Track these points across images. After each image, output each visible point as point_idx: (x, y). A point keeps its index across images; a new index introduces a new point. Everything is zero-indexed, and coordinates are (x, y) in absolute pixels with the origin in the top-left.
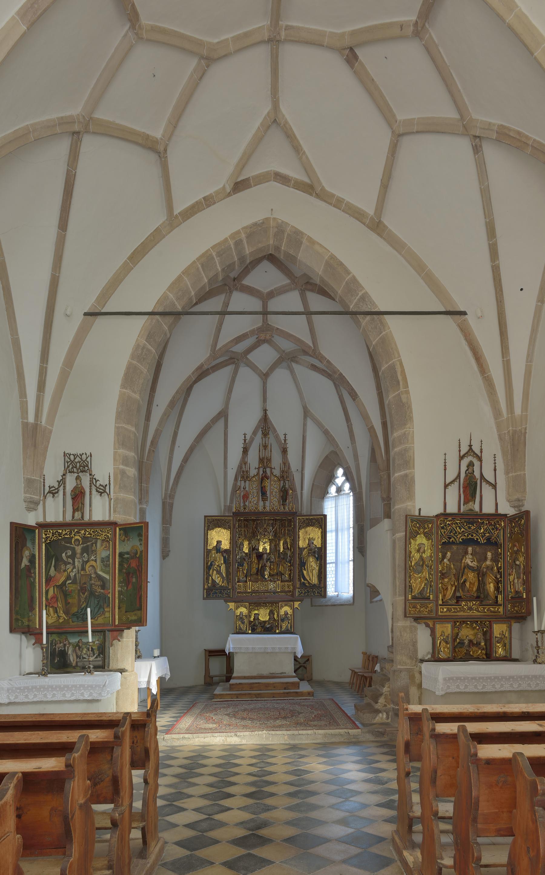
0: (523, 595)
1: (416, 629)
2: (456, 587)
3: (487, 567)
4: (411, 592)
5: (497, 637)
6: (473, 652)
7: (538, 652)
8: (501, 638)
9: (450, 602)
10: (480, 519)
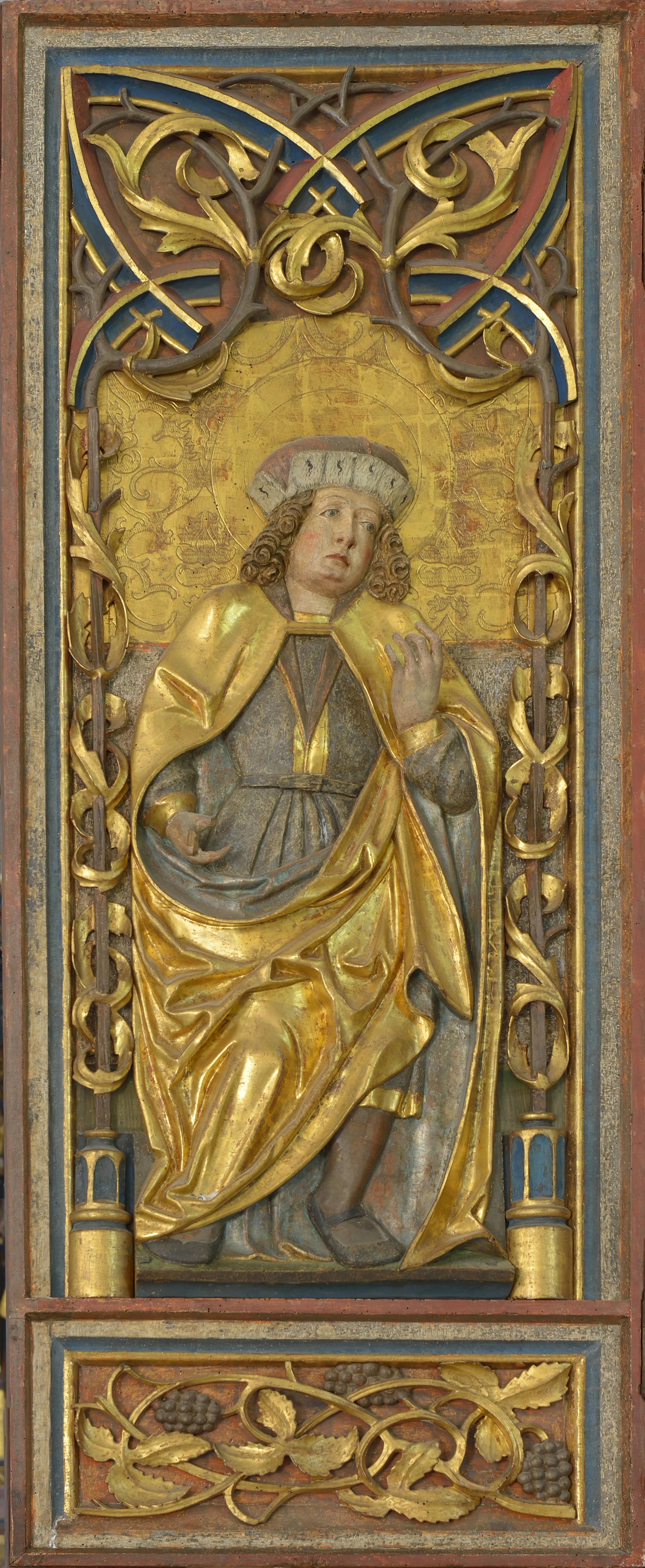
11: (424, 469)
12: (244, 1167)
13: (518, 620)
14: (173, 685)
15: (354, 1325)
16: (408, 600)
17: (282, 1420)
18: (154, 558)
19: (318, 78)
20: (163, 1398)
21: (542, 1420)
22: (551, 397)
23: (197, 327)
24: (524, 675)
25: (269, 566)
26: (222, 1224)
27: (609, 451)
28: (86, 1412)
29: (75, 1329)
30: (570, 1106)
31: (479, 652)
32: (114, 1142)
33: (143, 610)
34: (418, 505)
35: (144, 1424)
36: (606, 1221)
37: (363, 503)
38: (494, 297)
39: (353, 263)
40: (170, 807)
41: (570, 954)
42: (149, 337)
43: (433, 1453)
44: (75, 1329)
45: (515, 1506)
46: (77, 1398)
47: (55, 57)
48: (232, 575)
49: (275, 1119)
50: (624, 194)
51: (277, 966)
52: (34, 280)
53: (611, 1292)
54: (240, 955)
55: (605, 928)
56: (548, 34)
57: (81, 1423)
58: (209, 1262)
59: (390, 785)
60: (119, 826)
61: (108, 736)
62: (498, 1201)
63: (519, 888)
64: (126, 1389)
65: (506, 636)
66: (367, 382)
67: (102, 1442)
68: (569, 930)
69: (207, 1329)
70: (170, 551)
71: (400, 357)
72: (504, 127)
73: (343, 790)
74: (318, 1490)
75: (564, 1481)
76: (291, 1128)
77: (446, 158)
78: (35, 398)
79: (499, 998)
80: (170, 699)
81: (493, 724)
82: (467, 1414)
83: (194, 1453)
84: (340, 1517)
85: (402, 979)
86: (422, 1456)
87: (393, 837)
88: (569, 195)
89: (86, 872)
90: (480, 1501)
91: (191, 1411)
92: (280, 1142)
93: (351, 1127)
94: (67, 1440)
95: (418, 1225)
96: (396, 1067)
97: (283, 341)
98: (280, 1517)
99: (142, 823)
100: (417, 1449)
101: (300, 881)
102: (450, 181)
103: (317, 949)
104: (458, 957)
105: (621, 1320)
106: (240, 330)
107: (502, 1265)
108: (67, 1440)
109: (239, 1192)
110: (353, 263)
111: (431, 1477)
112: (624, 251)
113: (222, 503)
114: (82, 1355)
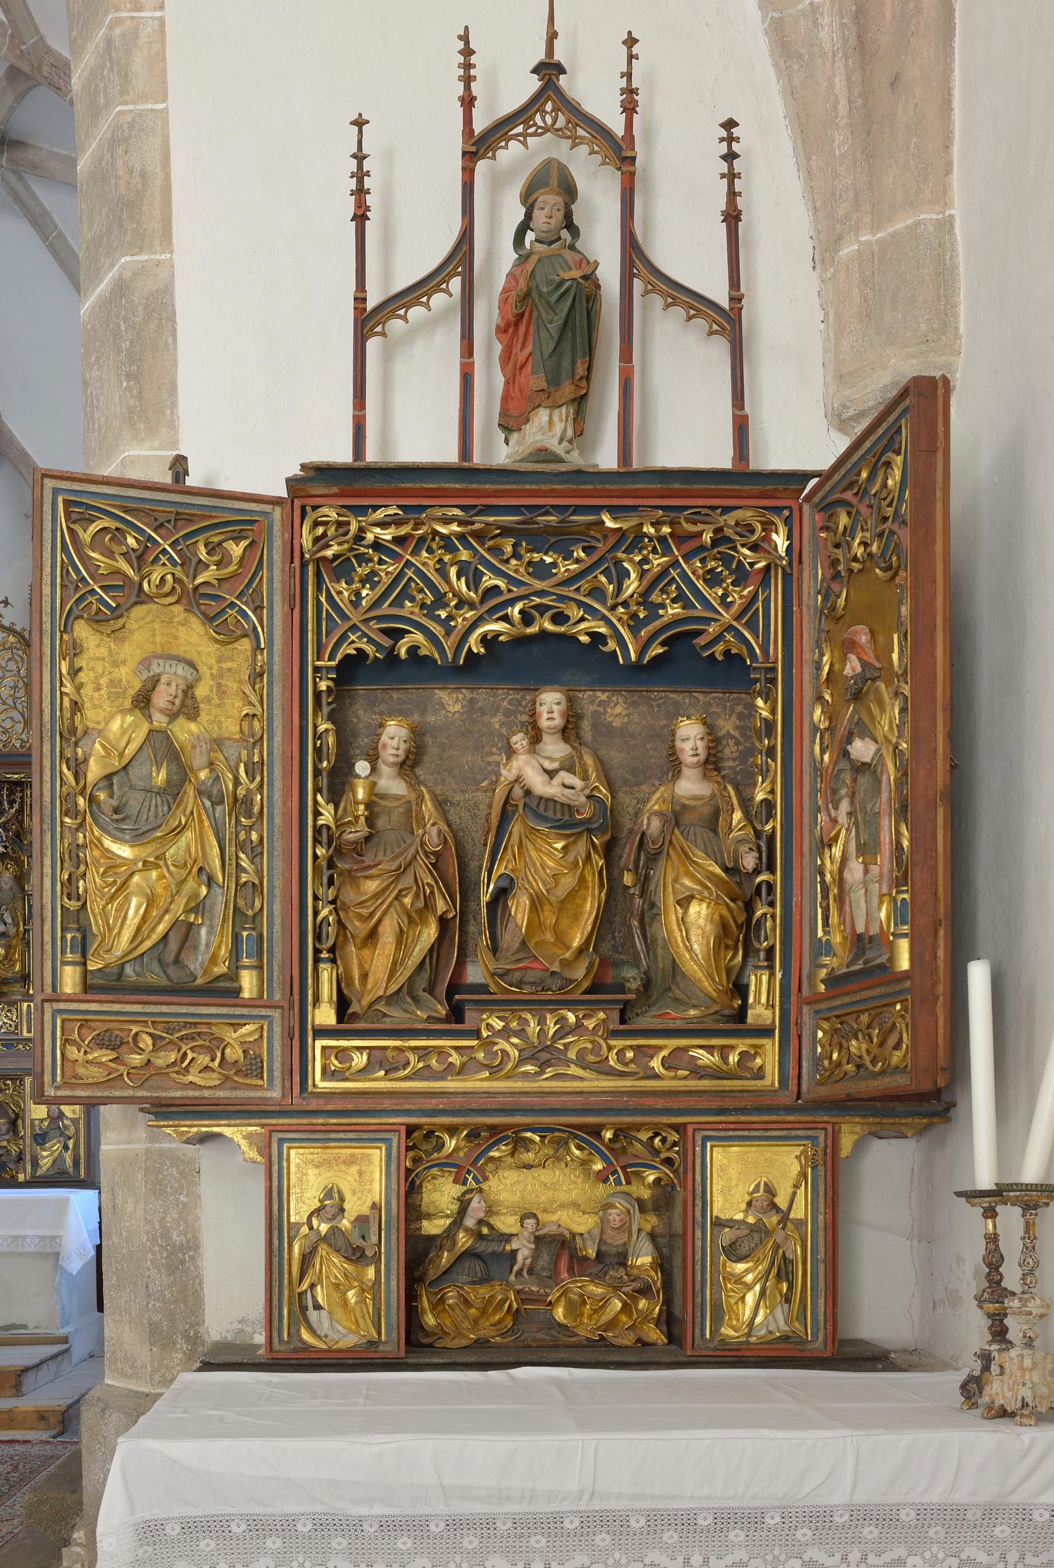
0: (892, 959)
1: (190, 1173)
2: (443, 923)
3: (677, 816)
4: (83, 948)
5: (730, 1223)
6: (574, 1309)
7: (999, 1333)
8: (759, 1230)
9: (396, 1016)
10: (612, 510)
11: (205, 669)
12: (132, 942)
13: (241, 731)
14: (103, 746)
15: (176, 1007)
16: (199, 719)
17: (147, 1044)
18: (96, 694)
19: (163, 512)
20: (98, 1035)
21: (251, 1046)
22: (255, 646)
23: (114, 605)
24: (244, 753)
25: (143, 702)
26: (123, 965)
27: (277, 668)
28: (67, 1040)
29: (62, 1006)
30: (262, 923)
31: (227, 742)
32: (78, 930)
33: (91, 715)
34: (202, 683)
35: (91, 1045)
36: (276, 968)
37: (180, 681)
38: (232, 605)
39: (176, 586)
40: (102, 796)
41: (262, 863)
42: (94, 606)
43: (208, 1058)
44: (62, 1006)
45: (240, 1080)
46: (63, 1034)
47: (56, 491)
48: (128, 704)
49: (144, 923)
50: (283, 571)
51: (145, 862)
52: (47, 579)
53: (277, 996)
54: (131, 857)
55: (275, 854)
56: (253, 506)
57: (64, 1044)
58: (117, 980)
59: (191, 792)
60: (81, 801)
61: (77, 765)
62: (234, 959)
63: (242, 836)
64: (84, 1031)
65: (237, 736)
66: (182, 631)
67: (73, 1052)
68: (262, 853)
69: (117, 1007)
70: (102, 692)
71: (196, 624)
72: (237, 539)
73: (173, 792)
74: (162, 1073)
75: (259, 1070)
76: (150, 928)
77: (214, 548)
78: (47, 626)
79: (234, 879)
80: (102, 752)
81: (232, 772)
82: (220, 1043)
83: (111, 1057)
84: (171, 1084)
85: (195, 870)
86: (204, 1059)
87: (192, 813)
88: (262, 568)
89: (67, 820)
90: (227, 1078)
91: (110, 1040)
92: (146, 933)
93: (175, 928)
94: (58, 1051)
95: (202, 967)
96: (193, 905)
97: (149, 613)
98: (146, 1084)
99: (90, 801)
100: (201, 1057)
101: (155, 829)
102: (215, 558)
103: (161, 857)
104: (218, 862)
105: (282, 1007)
106: (131, 607)
107: (235, 985)
108: (58, 1051)
109: (130, 952)
110: (176, 586)
111: (207, 1068)
112: (283, 593)
113: (124, 675)
114: (65, 1017)
